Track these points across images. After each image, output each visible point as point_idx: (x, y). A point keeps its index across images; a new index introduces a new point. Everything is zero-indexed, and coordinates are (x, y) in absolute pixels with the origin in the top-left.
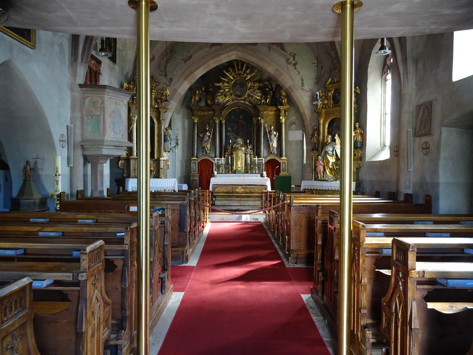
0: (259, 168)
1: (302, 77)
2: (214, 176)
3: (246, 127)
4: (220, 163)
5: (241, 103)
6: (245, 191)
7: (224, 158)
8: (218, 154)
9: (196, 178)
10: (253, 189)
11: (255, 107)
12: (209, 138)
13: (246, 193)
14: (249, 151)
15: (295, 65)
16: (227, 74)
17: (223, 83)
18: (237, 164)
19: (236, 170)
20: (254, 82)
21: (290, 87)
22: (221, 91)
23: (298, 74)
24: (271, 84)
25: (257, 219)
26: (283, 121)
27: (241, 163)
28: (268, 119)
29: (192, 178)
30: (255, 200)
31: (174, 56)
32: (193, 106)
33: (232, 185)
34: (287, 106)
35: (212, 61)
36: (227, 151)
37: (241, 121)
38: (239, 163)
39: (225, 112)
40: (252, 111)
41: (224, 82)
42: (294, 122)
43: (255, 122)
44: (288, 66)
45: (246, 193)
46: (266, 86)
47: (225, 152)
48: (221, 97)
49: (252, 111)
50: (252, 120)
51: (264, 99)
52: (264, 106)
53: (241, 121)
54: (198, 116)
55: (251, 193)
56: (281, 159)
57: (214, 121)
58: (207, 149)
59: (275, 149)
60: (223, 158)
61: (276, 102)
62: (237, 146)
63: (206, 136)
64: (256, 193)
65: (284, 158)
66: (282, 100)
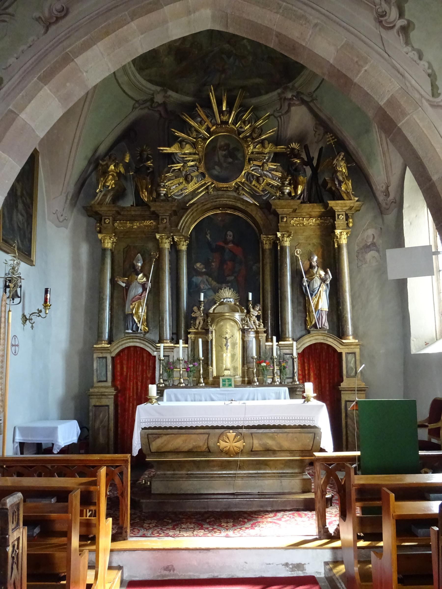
0: (282, 370)
1: (430, 66)
2: (146, 399)
3: (241, 257)
4: (173, 357)
5: (229, 197)
6: (248, 448)
7: (186, 342)
8: (167, 333)
9: (104, 401)
10: (273, 438)
11: (266, 206)
12: (144, 289)
13: (252, 452)
14: (254, 322)
15: (405, 30)
16: (192, 123)
17: (182, 147)
18: (220, 359)
19: (217, 378)
20: (262, 142)
21: (392, 102)
22: (179, 166)
23: (416, 57)
24: (306, 148)
25: (299, 566)
26: (344, 241)
27: (233, 356)
28: (301, 238)
29: (94, 402)
30: (282, 476)
31: (10, 10)
32: (100, 203)
33: (207, 427)
34: (353, 202)
35: (133, 25)
36: (192, 324)
37: (231, 245)
38: (227, 356)
39: (189, 224)
40: (258, 216)
41: (182, 143)
42: (373, 244)
43: (267, 246)
44: (384, 33)
45: (252, 452)
46: (294, 154)
47: (188, 326)
48: (176, 181)
49: (258, 216)
50: (258, 242)
51: (290, 184)
52: (292, 202)
53: (231, 245)
54: (115, 232)
55: (268, 451)
56: (342, 344)
57: (157, 243)
58: (139, 318)
59: (325, 318)
60: (181, 344)
61: (321, 192)
62: (220, 309)
63: (134, 284)
64: (283, 451)
65: (351, 340)
66: (340, 183)
